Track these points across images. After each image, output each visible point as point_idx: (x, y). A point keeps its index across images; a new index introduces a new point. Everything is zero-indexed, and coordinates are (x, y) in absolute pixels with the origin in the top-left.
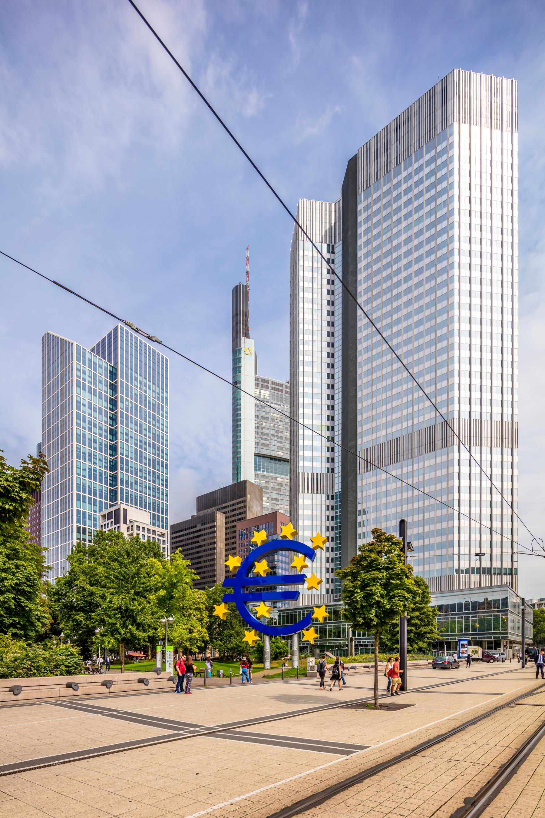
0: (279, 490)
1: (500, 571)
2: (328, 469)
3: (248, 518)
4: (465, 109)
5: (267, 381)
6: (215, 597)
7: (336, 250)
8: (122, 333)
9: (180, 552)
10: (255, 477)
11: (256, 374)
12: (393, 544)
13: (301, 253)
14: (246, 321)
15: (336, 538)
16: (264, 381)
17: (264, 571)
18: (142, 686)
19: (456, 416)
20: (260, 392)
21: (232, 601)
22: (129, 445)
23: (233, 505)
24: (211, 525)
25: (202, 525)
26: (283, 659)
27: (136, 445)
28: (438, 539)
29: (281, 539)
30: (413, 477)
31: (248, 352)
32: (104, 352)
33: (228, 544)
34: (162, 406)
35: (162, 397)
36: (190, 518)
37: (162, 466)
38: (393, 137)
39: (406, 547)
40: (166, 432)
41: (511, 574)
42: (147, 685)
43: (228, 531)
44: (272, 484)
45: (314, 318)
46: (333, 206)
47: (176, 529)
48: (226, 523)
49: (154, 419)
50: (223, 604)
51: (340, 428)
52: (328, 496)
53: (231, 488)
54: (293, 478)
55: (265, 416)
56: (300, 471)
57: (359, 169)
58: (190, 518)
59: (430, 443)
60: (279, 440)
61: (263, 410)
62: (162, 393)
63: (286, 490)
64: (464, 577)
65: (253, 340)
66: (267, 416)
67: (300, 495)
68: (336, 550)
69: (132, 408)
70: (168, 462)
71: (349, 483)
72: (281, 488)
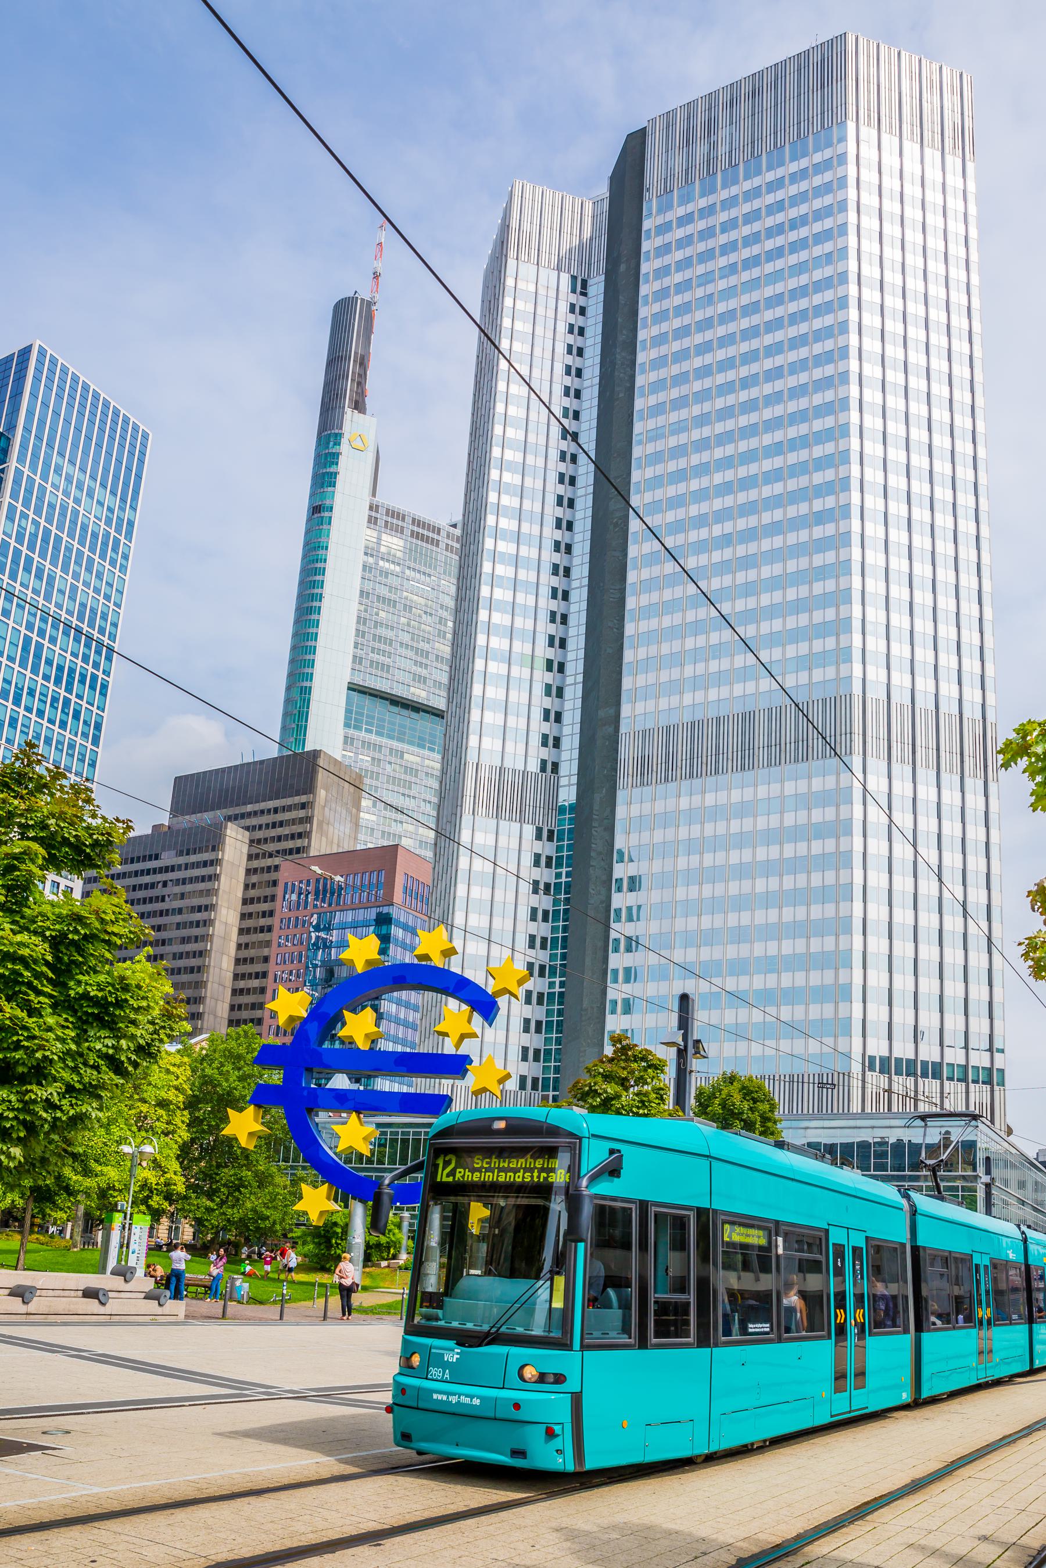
0: (410, 785)
1: (964, 1074)
2: (544, 763)
3: (313, 852)
4: (869, 102)
6: (209, 1071)
7: (592, 290)
8: (40, 362)
9: (149, 958)
10: (345, 743)
11: (374, 495)
13: (510, 282)
14: (360, 375)
16: (391, 513)
17: (367, 1035)
18: (93, 1305)
19: (857, 690)
20: (379, 539)
21: (276, 1103)
22: (11, 624)
23: (276, 811)
25: (181, 853)
26: (384, 1264)
27: (30, 627)
28: (815, 978)
29: (416, 961)
30: (755, 816)
31: (358, 444)
33: (250, 915)
34: (117, 542)
35: (120, 520)
36: (150, 832)
37: (93, 688)
38: (723, 117)
40: (115, 604)
41: (989, 1082)
42: (103, 1304)
43: (254, 879)
44: (388, 766)
45: (531, 418)
46: (589, 207)
48: (250, 857)
49: (89, 570)
50: (251, 1108)
52: (539, 830)
53: (274, 765)
54: (451, 771)
55: (388, 595)
56: (472, 757)
57: (648, 156)
59: (796, 742)
60: (419, 659)
61: (384, 580)
62: (122, 509)
63: (427, 790)
64: (876, 1080)
65: (374, 420)
66: (393, 597)
67: (467, 819)
68: (553, 973)
69: (34, 536)
70: (110, 680)
71: (596, 807)
72: (413, 779)
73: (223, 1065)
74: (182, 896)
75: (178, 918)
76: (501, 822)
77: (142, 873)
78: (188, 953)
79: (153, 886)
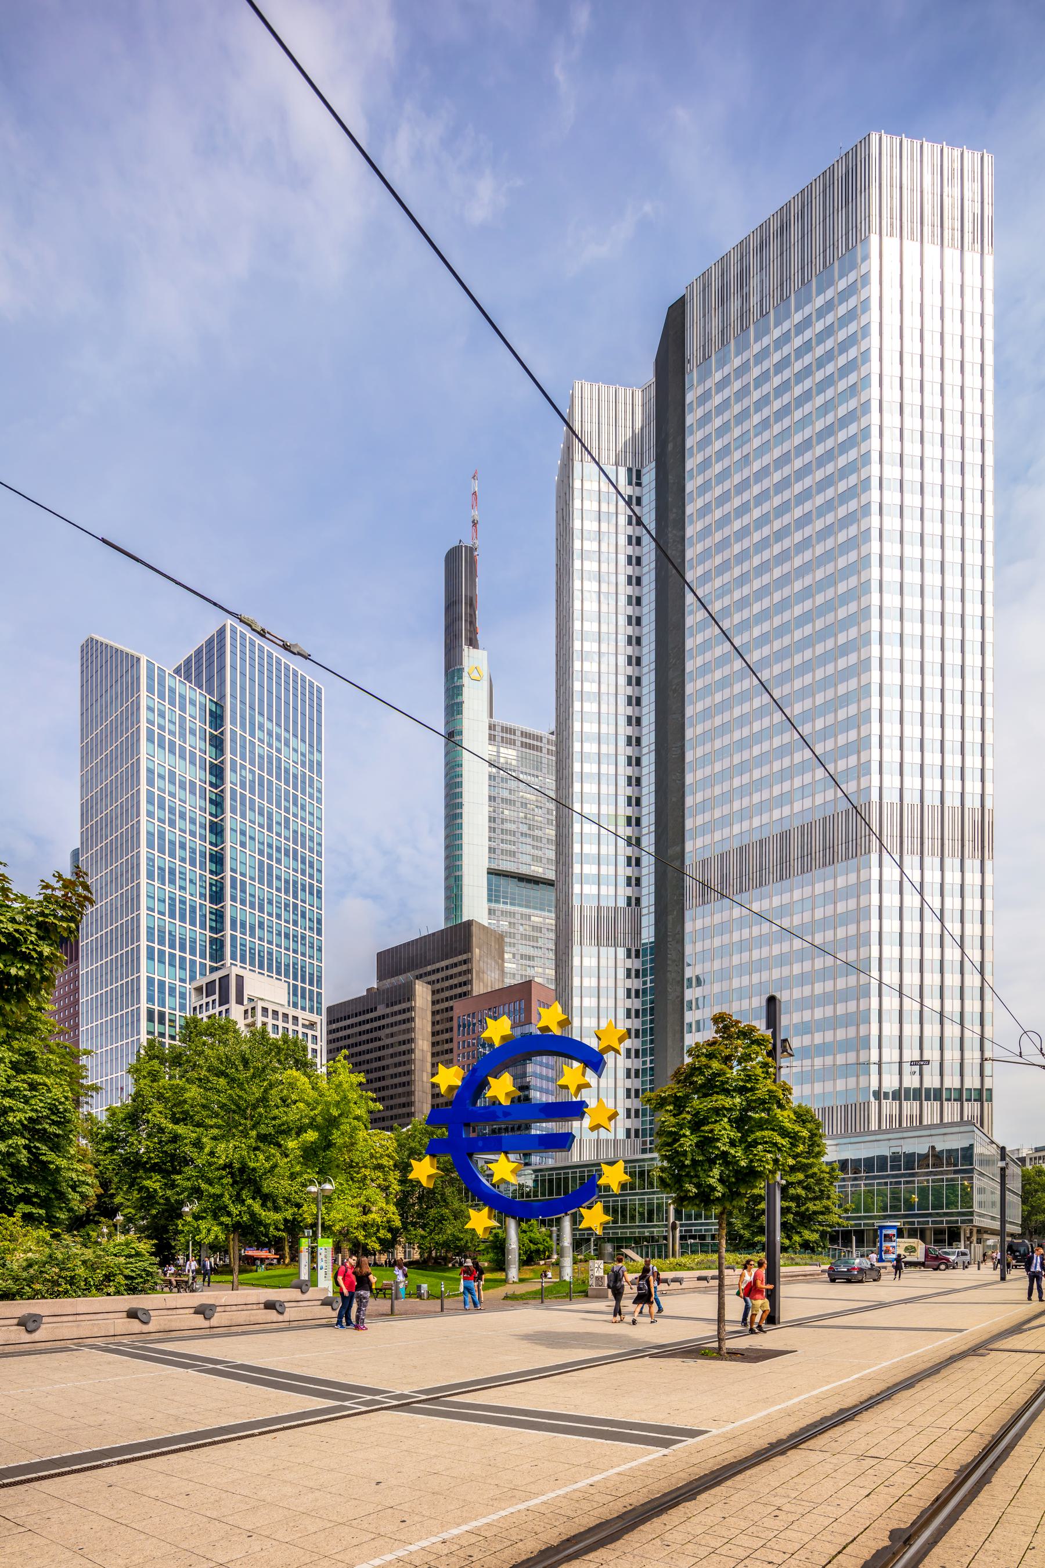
0: (536, 939)
2: (629, 898)
3: (475, 994)
4: (891, 209)
5: (511, 731)
6: (413, 1145)
7: (645, 480)
8: (233, 639)
9: (345, 1058)
10: (490, 914)
11: (491, 717)
13: (577, 484)
14: (471, 615)
16: (506, 730)
17: (507, 1094)
18: (272, 1315)
19: (875, 797)
20: (498, 752)
21: (444, 1152)
22: (248, 852)
23: (447, 968)
24: (404, 1006)
25: (387, 1006)
26: (542, 1262)
27: (261, 853)
28: (841, 1034)
29: (539, 1033)
30: (792, 915)
31: (475, 675)
32: (199, 675)
33: (438, 1043)
34: (311, 779)
35: (311, 761)
36: (365, 993)
37: (311, 893)
38: (754, 263)
39: (779, 1049)
40: (318, 829)
41: (980, 1099)
42: (282, 1313)
43: (438, 1018)
44: (521, 928)
45: (602, 610)
46: (638, 395)
47: (337, 1015)
48: (433, 1003)
49: (295, 804)
50: (428, 1157)
51: (653, 820)
52: (629, 951)
53: (442, 935)
54: (562, 915)
55: (509, 797)
56: (576, 902)
57: (688, 325)
58: (365, 993)
59: (824, 849)
60: (535, 843)
61: (505, 785)
62: (311, 753)
63: (548, 939)
64: (889, 1107)
65: (485, 653)
66: (512, 797)
67: (576, 949)
68: (644, 1055)
69: (253, 782)
70: (323, 886)
71: (670, 926)
72: (539, 935)
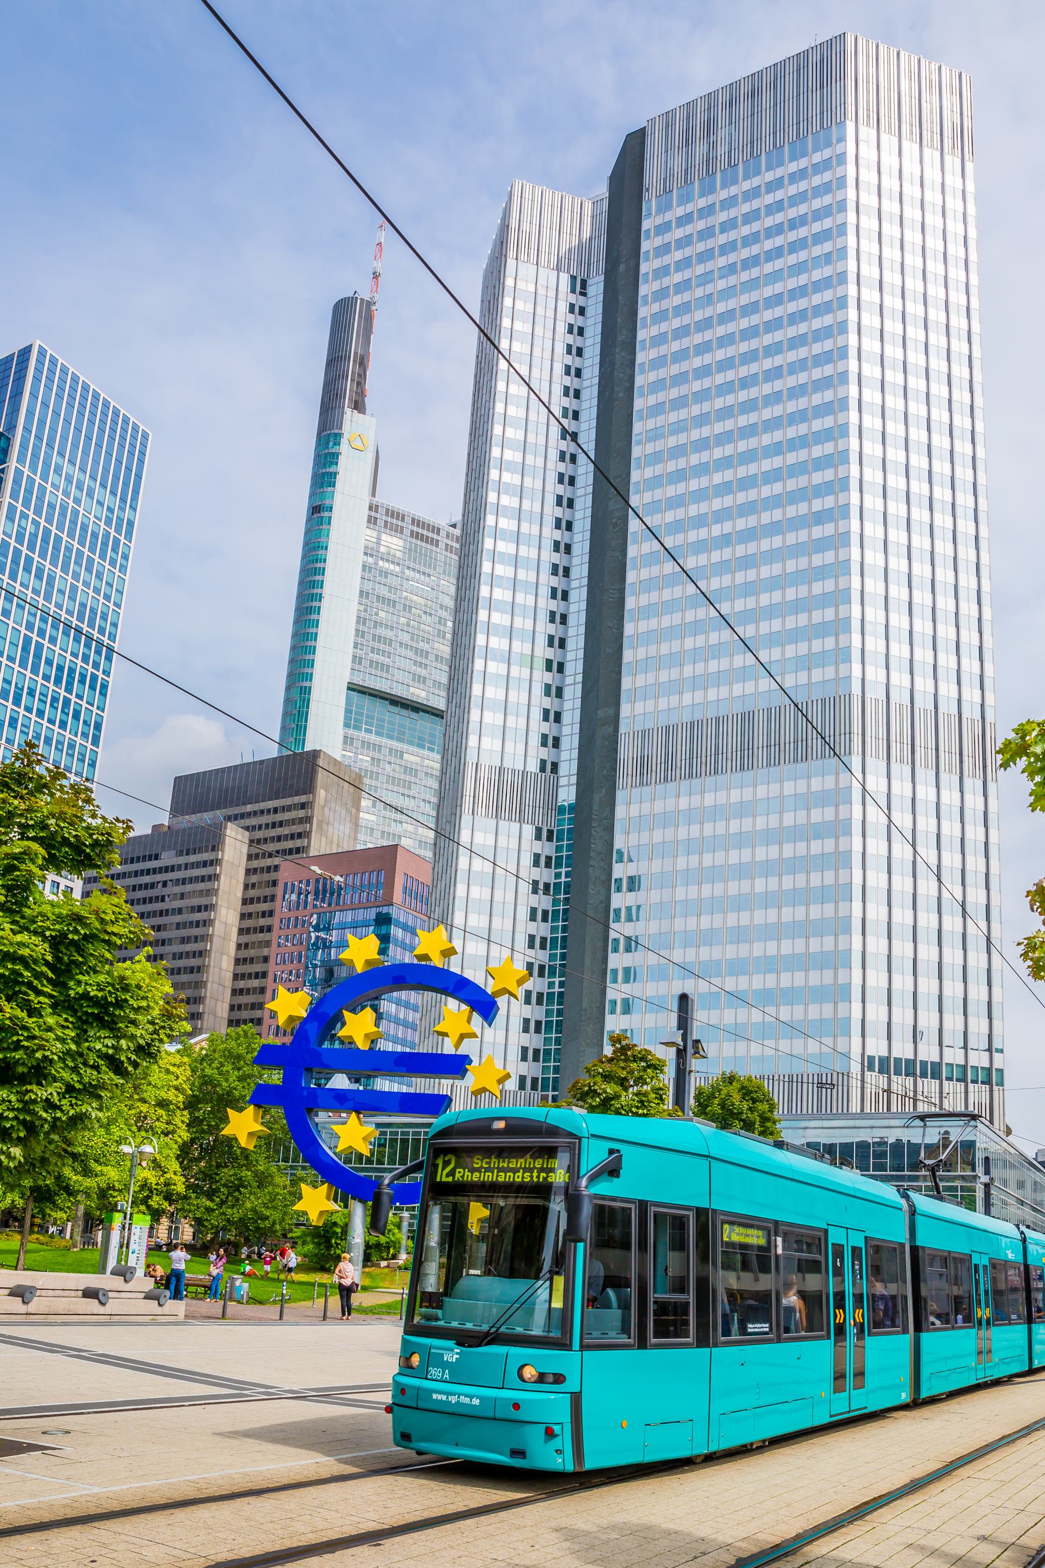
0: (409, 785)
2: (543, 763)
3: (313, 852)
4: (868, 102)
6: (208, 1071)
7: (591, 290)
8: (40, 362)
9: (149, 958)
10: (345, 743)
11: (374, 495)
12: (649, 1067)
13: (509, 282)
14: (359, 375)
15: (547, 1052)
16: (391, 513)
17: (366, 1035)
18: (93, 1305)
19: (856, 690)
20: (379, 539)
21: (276, 1103)
22: (11, 624)
23: (276, 811)
25: (181, 853)
26: (384, 1264)
27: (30, 627)
28: (815, 978)
29: (415, 961)
30: (754, 816)
31: (357, 444)
33: (250, 915)
34: (117, 542)
35: (120, 520)
36: (149, 832)
37: (92, 688)
38: (722, 117)
39: (690, 1050)
40: (115, 604)
41: (988, 1082)
42: (103, 1304)
43: (254, 879)
44: (387, 766)
45: (530, 418)
46: (588, 207)
48: (250, 857)
49: (89, 570)
50: (251, 1108)
52: (539, 830)
53: (274, 765)
54: (450, 771)
55: (387, 595)
56: (471, 757)
57: (647, 156)
59: (796, 742)
60: (419, 659)
61: (383, 580)
62: (122, 509)
63: (426, 790)
64: (875, 1080)
65: (374, 420)
66: (392, 597)
67: (466, 819)
68: (552, 973)
69: (34, 536)
70: (110, 680)
71: (596, 807)
72: (413, 779)
73: (222, 1065)
74: (182, 896)
75: (178, 918)
76: (501, 822)
77: (142, 873)
78: (187, 953)
79: (153, 886)
